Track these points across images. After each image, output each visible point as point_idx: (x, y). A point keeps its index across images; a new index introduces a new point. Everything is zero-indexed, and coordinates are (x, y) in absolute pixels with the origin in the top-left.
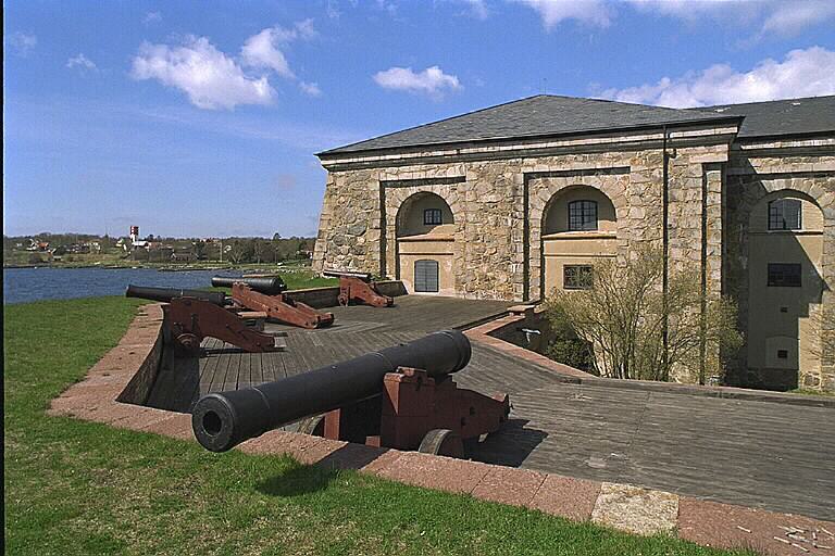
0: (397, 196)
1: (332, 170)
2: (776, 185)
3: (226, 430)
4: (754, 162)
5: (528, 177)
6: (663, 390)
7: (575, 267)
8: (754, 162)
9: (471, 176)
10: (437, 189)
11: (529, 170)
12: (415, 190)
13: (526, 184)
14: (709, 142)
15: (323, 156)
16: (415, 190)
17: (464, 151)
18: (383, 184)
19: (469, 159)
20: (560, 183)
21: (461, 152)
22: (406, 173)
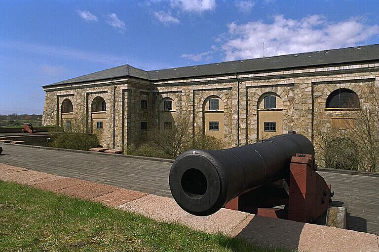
0: (61, 100)
1: (47, 91)
2: (164, 96)
3: (212, 192)
4: (159, 88)
5: (88, 94)
6: (103, 154)
7: (213, 122)
8: (159, 88)
9: (76, 94)
10: (101, 95)
11: (87, 92)
12: (65, 98)
13: (87, 96)
14: (123, 83)
15: (44, 87)
16: (65, 98)
17: (240, 77)
18: (58, 96)
19: (75, 88)
20: (95, 96)
21: (73, 86)
22: (63, 93)
